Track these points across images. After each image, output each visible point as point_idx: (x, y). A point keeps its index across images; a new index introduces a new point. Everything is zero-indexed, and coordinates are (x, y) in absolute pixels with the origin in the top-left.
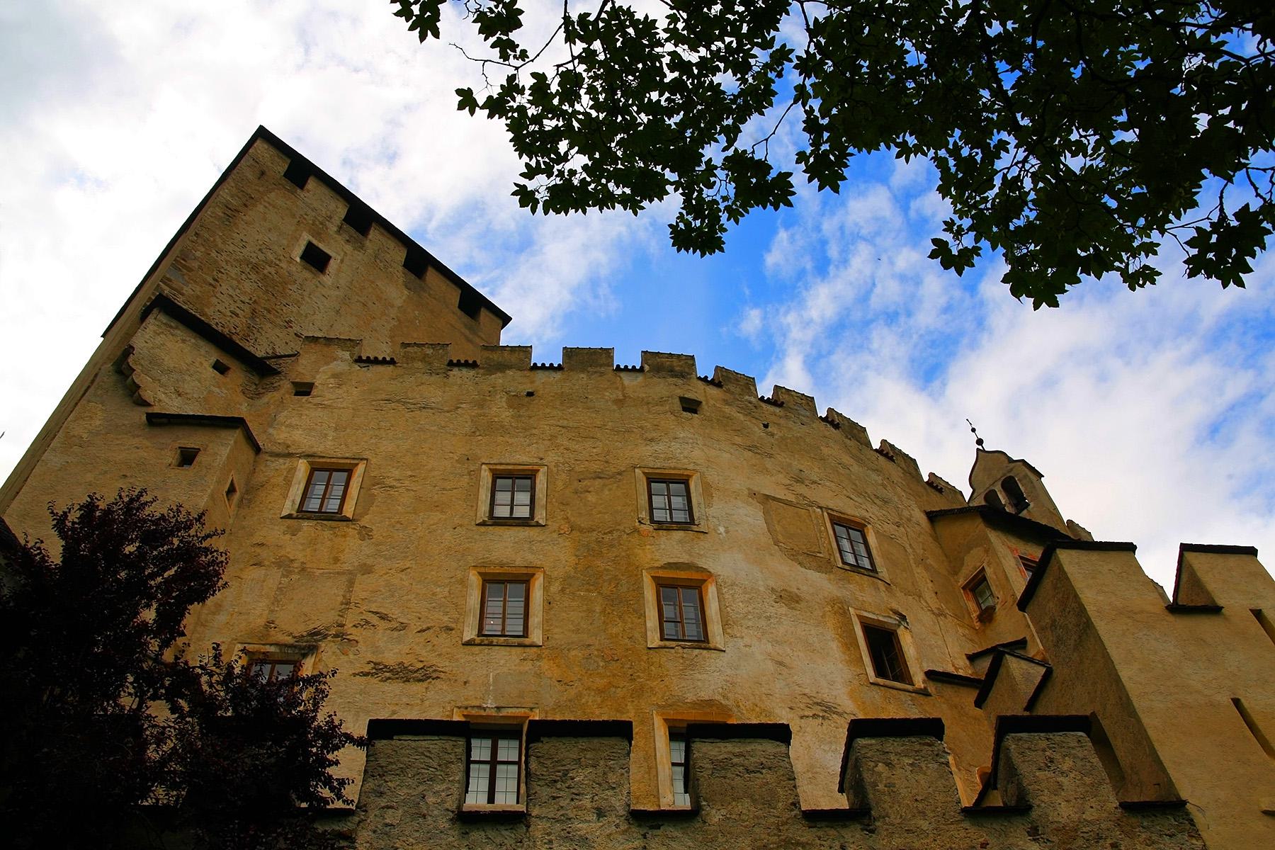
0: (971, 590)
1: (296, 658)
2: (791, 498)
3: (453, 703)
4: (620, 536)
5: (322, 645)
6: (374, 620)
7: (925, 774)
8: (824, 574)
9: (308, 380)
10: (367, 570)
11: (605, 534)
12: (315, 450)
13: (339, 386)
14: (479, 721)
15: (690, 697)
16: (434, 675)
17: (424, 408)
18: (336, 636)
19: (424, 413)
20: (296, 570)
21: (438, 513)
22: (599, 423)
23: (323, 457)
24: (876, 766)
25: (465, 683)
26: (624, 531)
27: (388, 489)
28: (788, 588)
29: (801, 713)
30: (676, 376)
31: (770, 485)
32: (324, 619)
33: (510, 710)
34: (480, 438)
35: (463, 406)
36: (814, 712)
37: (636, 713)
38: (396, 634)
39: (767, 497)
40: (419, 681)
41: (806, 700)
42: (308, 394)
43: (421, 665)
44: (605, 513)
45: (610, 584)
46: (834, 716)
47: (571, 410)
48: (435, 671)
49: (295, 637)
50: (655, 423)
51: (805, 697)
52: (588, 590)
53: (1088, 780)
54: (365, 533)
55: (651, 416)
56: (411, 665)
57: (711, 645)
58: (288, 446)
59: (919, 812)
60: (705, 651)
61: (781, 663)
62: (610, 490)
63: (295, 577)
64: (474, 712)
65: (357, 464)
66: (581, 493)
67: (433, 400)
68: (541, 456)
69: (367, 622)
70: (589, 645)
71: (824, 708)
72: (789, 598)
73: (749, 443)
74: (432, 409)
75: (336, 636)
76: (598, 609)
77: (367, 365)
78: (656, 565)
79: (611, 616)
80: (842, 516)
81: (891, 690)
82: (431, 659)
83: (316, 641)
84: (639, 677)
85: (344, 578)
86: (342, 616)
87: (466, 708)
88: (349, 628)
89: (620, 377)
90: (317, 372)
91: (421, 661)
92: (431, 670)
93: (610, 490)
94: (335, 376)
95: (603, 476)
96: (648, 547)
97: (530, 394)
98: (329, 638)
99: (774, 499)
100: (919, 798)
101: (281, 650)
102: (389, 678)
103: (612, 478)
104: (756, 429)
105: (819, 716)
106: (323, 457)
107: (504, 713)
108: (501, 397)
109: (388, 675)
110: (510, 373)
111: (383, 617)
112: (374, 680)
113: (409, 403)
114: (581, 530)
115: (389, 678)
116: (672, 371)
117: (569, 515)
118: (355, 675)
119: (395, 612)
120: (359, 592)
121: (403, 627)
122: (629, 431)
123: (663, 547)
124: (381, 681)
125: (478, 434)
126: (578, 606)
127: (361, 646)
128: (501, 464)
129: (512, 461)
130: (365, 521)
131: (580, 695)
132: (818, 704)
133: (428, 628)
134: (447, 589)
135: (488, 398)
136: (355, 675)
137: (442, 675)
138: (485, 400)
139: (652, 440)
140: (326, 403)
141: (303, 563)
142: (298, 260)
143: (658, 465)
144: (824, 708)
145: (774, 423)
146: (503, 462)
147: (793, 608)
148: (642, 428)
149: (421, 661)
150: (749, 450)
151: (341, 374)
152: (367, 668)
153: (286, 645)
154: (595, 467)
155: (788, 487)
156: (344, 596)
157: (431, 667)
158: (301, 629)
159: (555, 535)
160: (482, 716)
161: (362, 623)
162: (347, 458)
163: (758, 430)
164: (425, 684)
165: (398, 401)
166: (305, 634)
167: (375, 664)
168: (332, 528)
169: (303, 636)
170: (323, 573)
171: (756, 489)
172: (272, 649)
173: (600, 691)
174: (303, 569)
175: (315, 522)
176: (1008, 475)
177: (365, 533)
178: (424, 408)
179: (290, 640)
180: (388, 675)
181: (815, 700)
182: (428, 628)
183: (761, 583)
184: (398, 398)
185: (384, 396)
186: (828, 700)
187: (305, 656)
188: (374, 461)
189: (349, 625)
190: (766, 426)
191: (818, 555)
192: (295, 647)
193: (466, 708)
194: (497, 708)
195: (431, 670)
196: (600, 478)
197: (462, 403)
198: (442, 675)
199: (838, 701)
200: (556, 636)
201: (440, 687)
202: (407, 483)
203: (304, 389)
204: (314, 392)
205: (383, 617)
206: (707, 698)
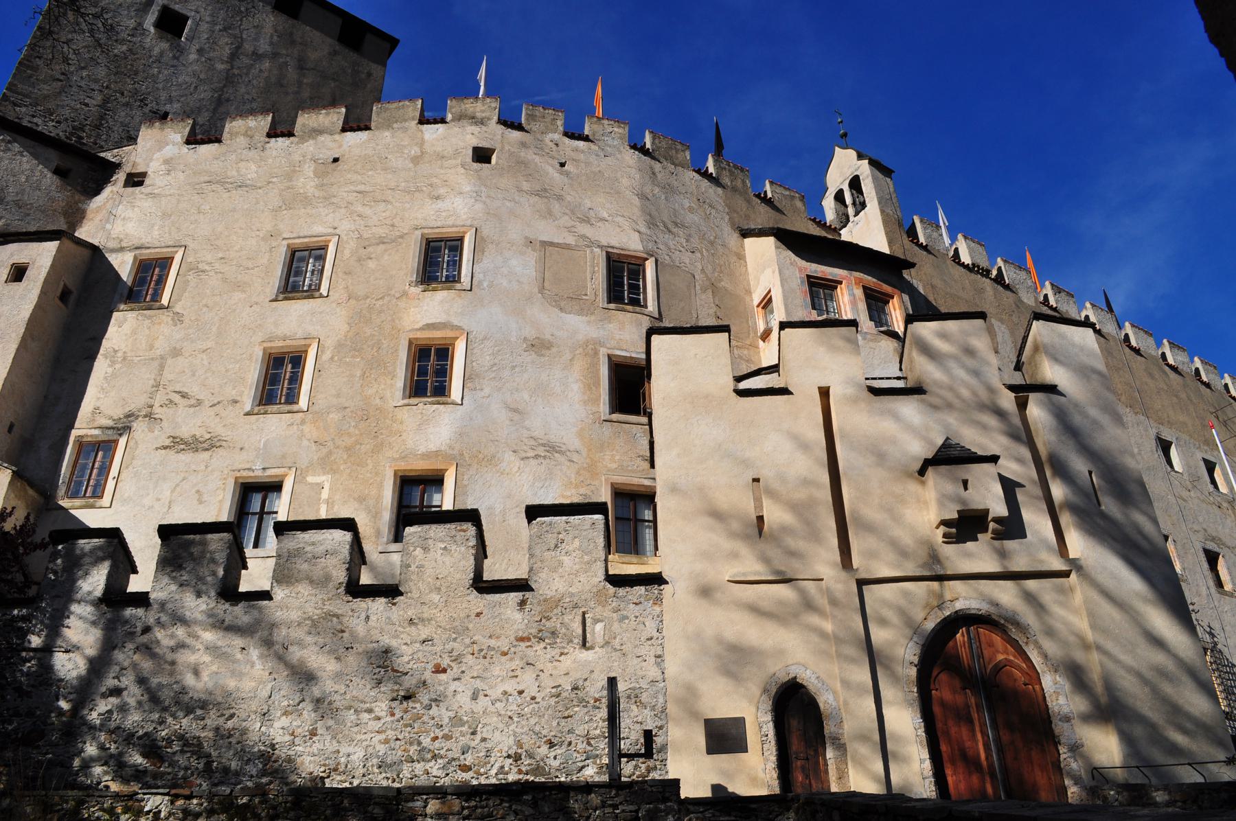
0: (763, 308)
1: (115, 438)
2: (571, 240)
3: (230, 467)
4: (390, 301)
5: (135, 425)
6: (177, 398)
7: (451, 556)
8: (584, 317)
9: (140, 169)
10: (176, 353)
11: (377, 300)
12: (143, 241)
13: (169, 172)
14: (250, 481)
15: (422, 449)
16: (218, 444)
17: (240, 186)
18: (145, 416)
19: (240, 191)
20: (119, 360)
21: (240, 293)
22: (393, 184)
23: (149, 248)
24: (414, 550)
25: (241, 449)
26: (394, 296)
27: (200, 273)
28: (542, 337)
29: (524, 455)
30: (476, 124)
31: (547, 231)
32: (137, 402)
33: (273, 470)
34: (285, 212)
35: (274, 180)
36: (536, 453)
37: (373, 466)
38: (192, 410)
39: (545, 244)
40: (207, 450)
41: (533, 442)
42: (140, 184)
43: (208, 436)
44: (380, 279)
45: (372, 349)
46: (556, 455)
47: (370, 173)
48: (220, 440)
49: (114, 420)
50: (445, 179)
51: (531, 440)
52: (353, 357)
53: (586, 558)
54: (178, 318)
55: (442, 171)
56: (201, 437)
57: (449, 400)
58: (121, 241)
59: (436, 588)
60: (442, 406)
61: (515, 410)
62: (390, 255)
63: (117, 366)
64: (245, 474)
65: (177, 252)
66: (364, 260)
67: (249, 176)
68: (336, 225)
69: (171, 401)
70: (345, 408)
71: (547, 448)
72: (539, 346)
73: (538, 187)
74: (246, 186)
75: (145, 416)
76: (359, 373)
77: (194, 146)
78: (416, 327)
79: (369, 379)
80: (622, 252)
81: (624, 425)
82: (219, 430)
83: (130, 422)
84: (382, 434)
85: (156, 364)
86: (151, 398)
87: (239, 471)
88: (157, 409)
89: (421, 131)
90: (151, 160)
91: (210, 433)
92: (216, 439)
93: (390, 255)
94: (167, 162)
95: (386, 241)
96: (412, 310)
97: (336, 160)
98: (140, 419)
99: (552, 244)
100: (440, 576)
101: (103, 432)
102: (184, 450)
103: (394, 241)
104: (550, 170)
105: (540, 456)
106: (149, 248)
107: (268, 473)
108: (309, 167)
109: (182, 446)
110: (321, 138)
111: (184, 396)
112: (171, 453)
113: (227, 182)
114: (357, 299)
115: (184, 450)
116: (473, 118)
117: (349, 284)
118: (157, 449)
119: (194, 390)
120: (168, 375)
121: (199, 403)
122: (419, 190)
123: (425, 308)
124: (177, 452)
125: (283, 208)
126: (343, 372)
127: (165, 424)
128: (299, 237)
129: (309, 233)
130: (178, 308)
131: (330, 453)
132: (543, 445)
133: (219, 403)
134: (237, 366)
135: (297, 169)
136: (157, 449)
137: (224, 444)
138: (294, 171)
139: (437, 198)
140: (156, 191)
141: (125, 352)
142: (152, 30)
143: (439, 224)
144: (547, 448)
145: (573, 160)
146: (302, 235)
147: (542, 355)
148: (431, 185)
149: (210, 433)
150: (537, 195)
151: (172, 159)
152: (167, 442)
153: (107, 428)
154: (381, 231)
155: (570, 229)
156: (155, 380)
157: (216, 437)
158: (118, 413)
159: (334, 305)
160: (251, 477)
161: (167, 402)
162: (168, 247)
163: (552, 172)
164: (209, 453)
165: (217, 183)
166: (122, 416)
167: (174, 438)
168: (150, 317)
169: (120, 419)
170: (141, 360)
171: (532, 237)
172: (97, 432)
173: (348, 449)
174: (124, 359)
175: (138, 312)
176: (855, 174)
177: (178, 318)
178: (240, 186)
179: (110, 423)
180: (182, 446)
181: (541, 442)
182: (219, 403)
183: (514, 333)
184: (218, 178)
185: (207, 178)
186: (554, 440)
187: (121, 435)
188: (191, 245)
189: (157, 405)
190: (562, 165)
191: (584, 297)
192: (113, 428)
193: (239, 471)
194: (264, 469)
195: (216, 439)
196: (384, 243)
197: (273, 177)
198: (224, 444)
199: (564, 440)
200: (320, 401)
201: (221, 453)
202: (217, 265)
203: (136, 180)
204: (147, 181)
205: (184, 396)
206: (434, 449)
